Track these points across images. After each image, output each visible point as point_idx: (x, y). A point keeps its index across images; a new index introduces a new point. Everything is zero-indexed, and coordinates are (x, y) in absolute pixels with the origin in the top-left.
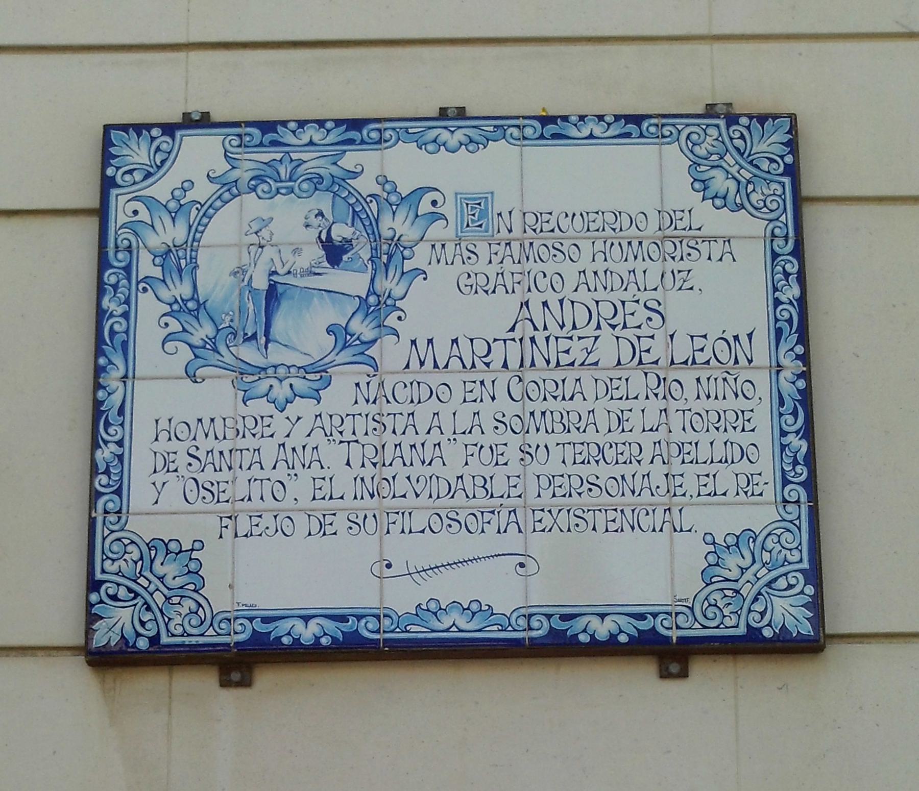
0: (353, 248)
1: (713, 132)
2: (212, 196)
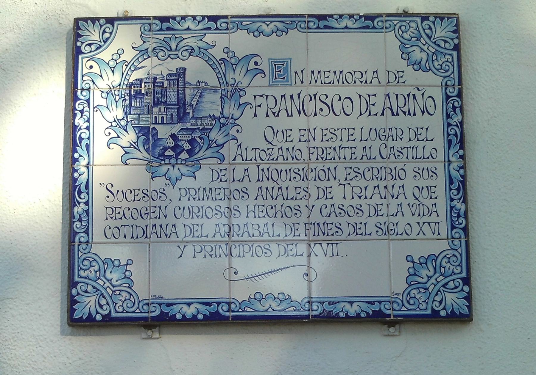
1: (413, 24)
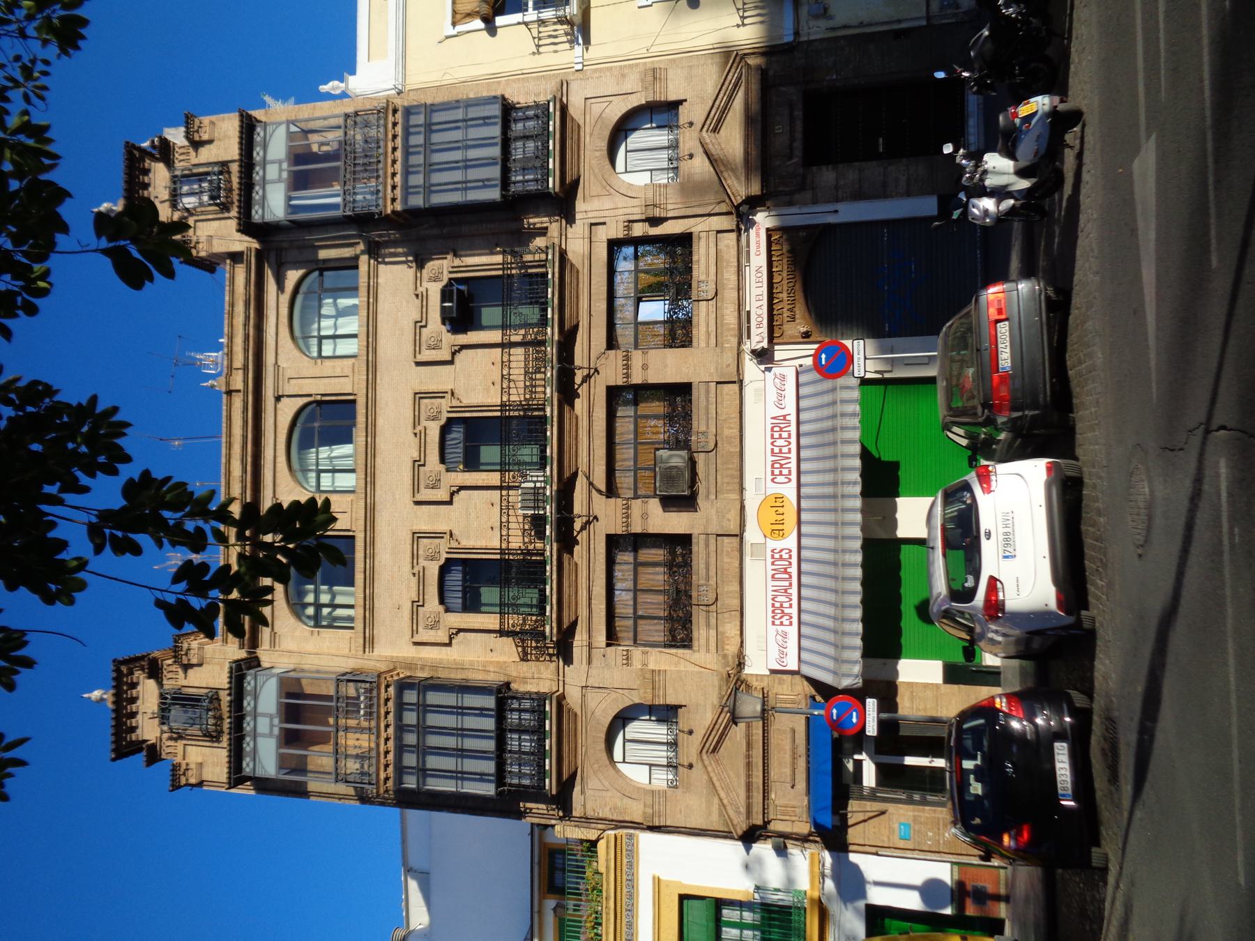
0: (805, 909)
2: (365, 633)
